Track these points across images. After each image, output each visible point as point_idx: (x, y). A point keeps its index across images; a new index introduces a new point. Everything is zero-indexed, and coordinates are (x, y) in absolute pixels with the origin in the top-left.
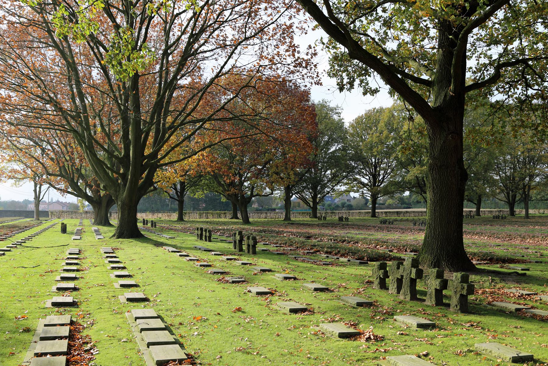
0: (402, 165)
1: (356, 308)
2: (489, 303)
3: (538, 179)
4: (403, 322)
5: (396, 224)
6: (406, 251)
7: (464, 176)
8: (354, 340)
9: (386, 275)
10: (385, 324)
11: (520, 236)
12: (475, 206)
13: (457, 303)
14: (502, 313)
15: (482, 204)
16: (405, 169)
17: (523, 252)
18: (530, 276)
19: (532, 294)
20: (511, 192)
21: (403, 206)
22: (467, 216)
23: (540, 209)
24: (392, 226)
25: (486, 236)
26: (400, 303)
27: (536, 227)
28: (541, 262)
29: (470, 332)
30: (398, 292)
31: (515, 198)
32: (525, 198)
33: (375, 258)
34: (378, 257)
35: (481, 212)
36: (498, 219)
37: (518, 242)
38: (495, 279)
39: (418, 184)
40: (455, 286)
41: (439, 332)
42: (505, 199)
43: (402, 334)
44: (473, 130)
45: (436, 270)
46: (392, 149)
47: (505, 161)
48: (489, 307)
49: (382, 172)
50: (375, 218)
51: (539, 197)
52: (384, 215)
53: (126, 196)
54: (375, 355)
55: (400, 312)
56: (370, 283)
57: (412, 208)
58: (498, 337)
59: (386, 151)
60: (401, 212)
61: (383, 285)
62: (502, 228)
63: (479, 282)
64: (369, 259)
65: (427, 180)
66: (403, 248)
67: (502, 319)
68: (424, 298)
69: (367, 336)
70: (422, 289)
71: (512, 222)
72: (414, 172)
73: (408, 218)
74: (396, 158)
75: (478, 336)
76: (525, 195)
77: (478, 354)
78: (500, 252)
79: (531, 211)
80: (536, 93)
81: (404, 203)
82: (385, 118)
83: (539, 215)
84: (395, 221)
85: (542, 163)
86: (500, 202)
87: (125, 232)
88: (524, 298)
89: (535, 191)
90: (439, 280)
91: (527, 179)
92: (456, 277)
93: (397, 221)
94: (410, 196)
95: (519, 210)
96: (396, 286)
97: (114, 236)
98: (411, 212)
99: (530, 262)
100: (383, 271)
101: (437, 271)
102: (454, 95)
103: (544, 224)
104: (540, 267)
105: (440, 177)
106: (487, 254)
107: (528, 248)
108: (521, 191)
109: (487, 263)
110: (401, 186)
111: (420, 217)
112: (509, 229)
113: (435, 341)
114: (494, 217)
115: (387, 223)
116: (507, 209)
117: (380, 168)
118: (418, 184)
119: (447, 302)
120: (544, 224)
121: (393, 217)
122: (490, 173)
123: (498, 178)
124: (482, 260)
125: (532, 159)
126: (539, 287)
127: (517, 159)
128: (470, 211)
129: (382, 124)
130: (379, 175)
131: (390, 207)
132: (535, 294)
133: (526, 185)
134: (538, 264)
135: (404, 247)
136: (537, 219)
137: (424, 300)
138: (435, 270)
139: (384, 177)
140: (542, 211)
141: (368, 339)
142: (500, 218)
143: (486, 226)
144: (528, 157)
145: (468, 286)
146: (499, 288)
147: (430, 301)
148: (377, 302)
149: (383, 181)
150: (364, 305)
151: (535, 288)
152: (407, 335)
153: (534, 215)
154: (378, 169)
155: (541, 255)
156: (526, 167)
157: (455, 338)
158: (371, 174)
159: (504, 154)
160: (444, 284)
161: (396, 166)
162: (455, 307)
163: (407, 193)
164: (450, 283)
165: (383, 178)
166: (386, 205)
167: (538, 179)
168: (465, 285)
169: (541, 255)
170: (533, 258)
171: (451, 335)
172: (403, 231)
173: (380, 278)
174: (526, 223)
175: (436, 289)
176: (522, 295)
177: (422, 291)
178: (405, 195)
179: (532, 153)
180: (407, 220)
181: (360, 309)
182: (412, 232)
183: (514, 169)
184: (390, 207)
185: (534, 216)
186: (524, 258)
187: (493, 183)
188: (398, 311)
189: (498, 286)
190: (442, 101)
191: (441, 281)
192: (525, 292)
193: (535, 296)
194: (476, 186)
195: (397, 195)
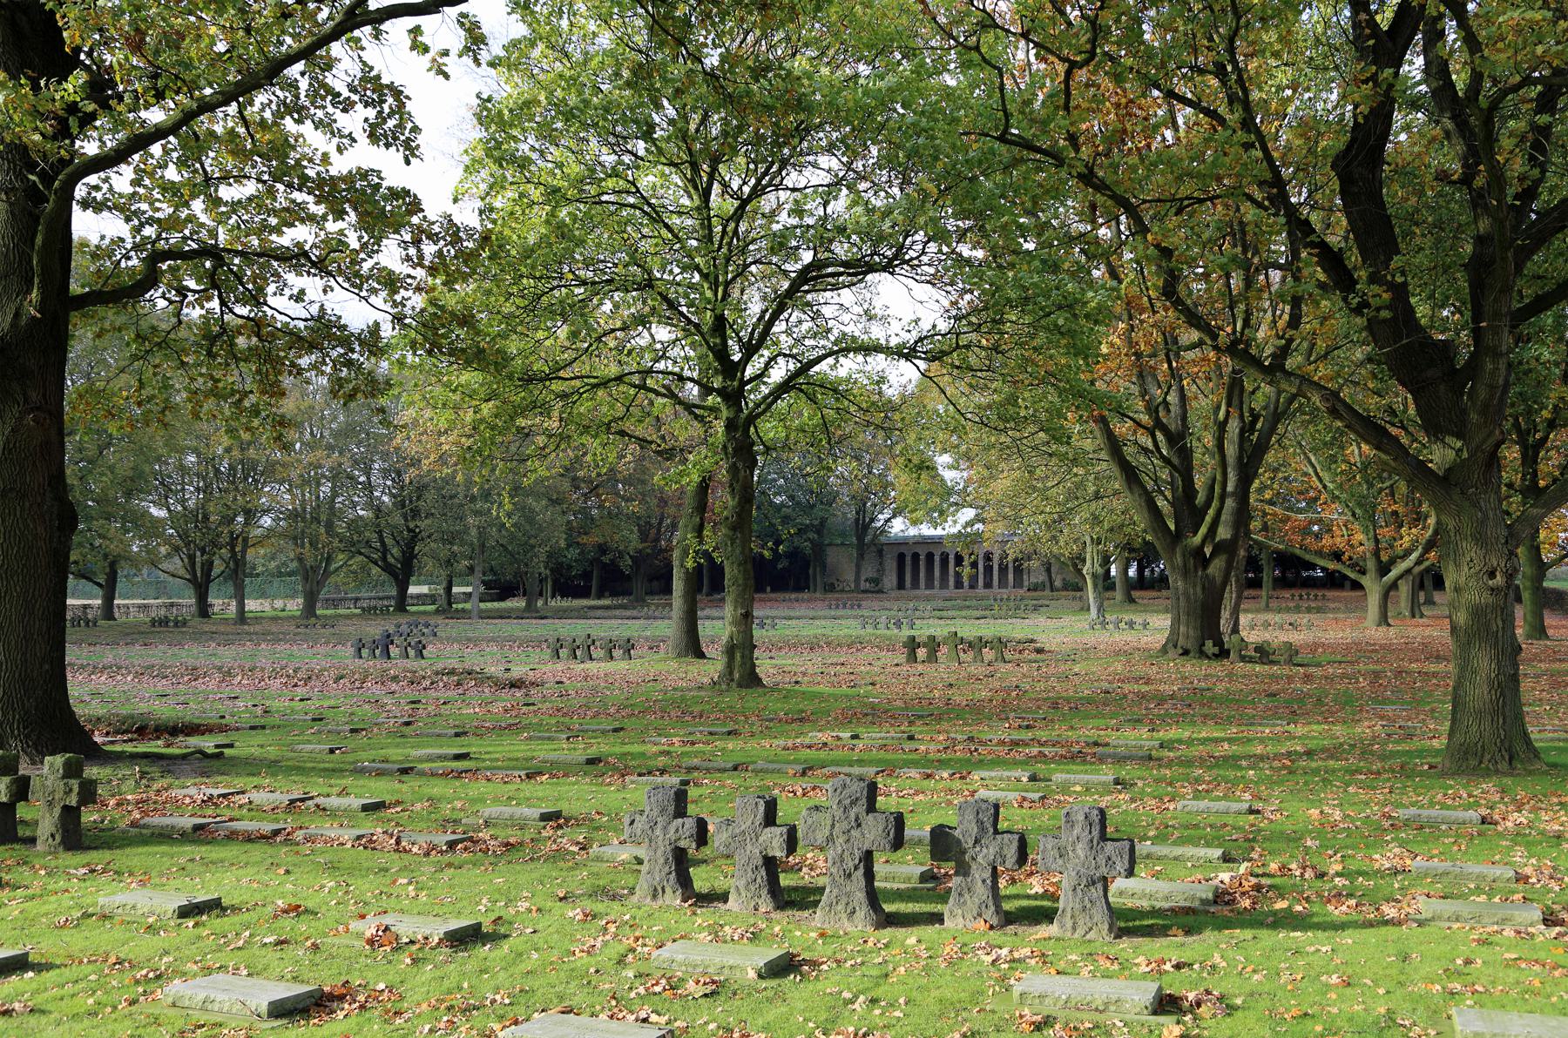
2: (134, 824)
3: (267, 521)
7: (67, 518)
11: (220, 669)
13: (53, 829)
14: (164, 836)
15: (121, 585)
18: (232, 758)
19: (232, 794)
20: (198, 553)
22: (76, 622)
23: (274, 597)
25: (130, 672)
27: (263, 646)
28: (263, 727)
29: (88, 883)
31: (210, 570)
32: (235, 571)
35: (116, 610)
37: (213, 685)
40: (51, 789)
42: (182, 572)
44: (91, 393)
47: (183, 469)
51: (273, 564)
58: (152, 881)
62: (176, 649)
71: (202, 633)
75: (107, 887)
76: (237, 562)
77: (104, 917)
78: (165, 711)
79: (251, 605)
80: (246, 324)
86: (171, 579)
91: (240, 519)
92: (52, 765)
95: (221, 602)
99: (238, 729)
102: (39, 315)
103: (281, 636)
104: (259, 738)
106: (131, 716)
107: (236, 698)
112: (192, 653)
116: (189, 600)
119: (28, 833)
120: (281, 636)
122: (141, 500)
123: (163, 513)
124: (117, 732)
127: (214, 466)
128: (85, 607)
132: (238, 793)
133: (238, 536)
134: (254, 732)
136: (266, 626)
140: (279, 604)
142: (172, 624)
143: (130, 648)
144: (242, 462)
145: (81, 785)
146: (158, 791)
155: (266, 712)
157: (53, 898)
162: (50, 840)
167: (267, 521)
168: (75, 784)
169: (266, 712)
171: (41, 895)
174: (238, 637)
176: (211, 797)
183: (204, 492)
185: (262, 618)
186: (223, 721)
187: (152, 529)
191: (12, 782)
192: (216, 792)
193: (237, 797)
194: (100, 536)
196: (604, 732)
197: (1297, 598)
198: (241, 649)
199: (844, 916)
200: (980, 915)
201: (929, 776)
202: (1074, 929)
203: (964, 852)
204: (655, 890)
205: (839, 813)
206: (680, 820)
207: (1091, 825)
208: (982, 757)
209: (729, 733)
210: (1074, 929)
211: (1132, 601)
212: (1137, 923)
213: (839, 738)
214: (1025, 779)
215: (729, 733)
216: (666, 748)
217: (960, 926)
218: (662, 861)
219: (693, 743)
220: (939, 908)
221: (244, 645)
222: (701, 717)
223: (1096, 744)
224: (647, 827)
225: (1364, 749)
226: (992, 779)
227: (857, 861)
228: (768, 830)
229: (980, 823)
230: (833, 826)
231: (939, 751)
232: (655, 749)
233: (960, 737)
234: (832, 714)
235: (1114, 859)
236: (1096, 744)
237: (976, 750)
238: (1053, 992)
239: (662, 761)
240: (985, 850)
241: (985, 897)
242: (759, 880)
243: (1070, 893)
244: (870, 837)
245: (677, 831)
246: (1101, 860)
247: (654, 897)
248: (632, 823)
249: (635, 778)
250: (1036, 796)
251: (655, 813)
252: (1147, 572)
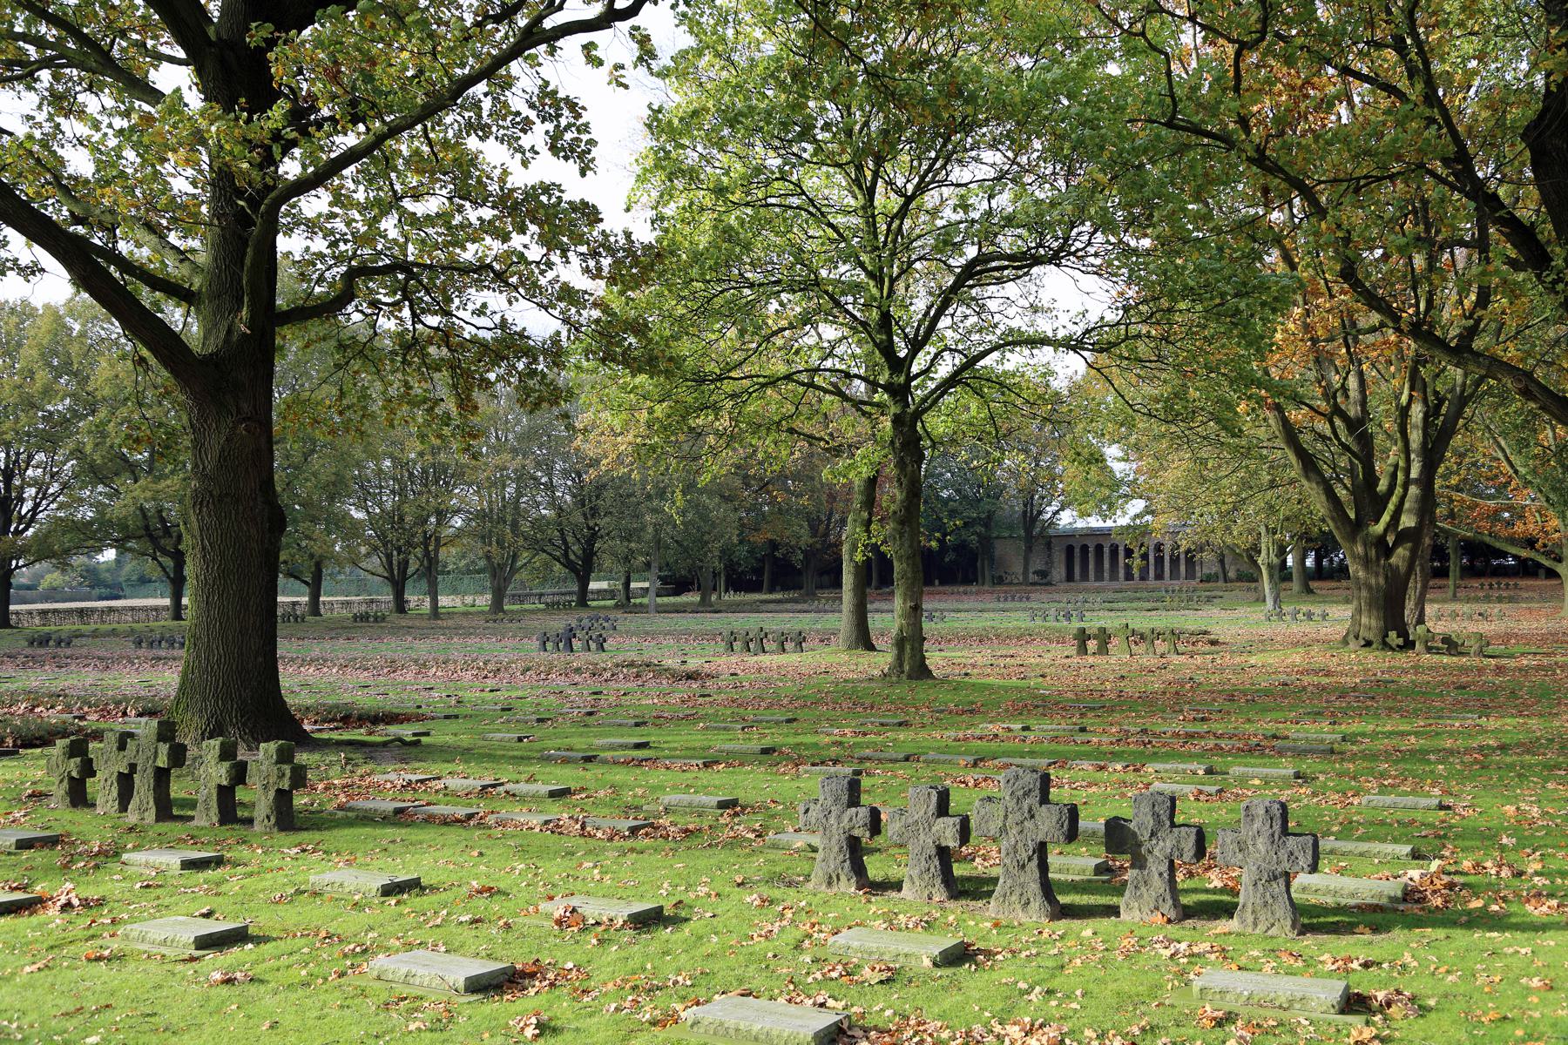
0: (94, 473)
1: (15, 854)
2: (341, 808)
3: (458, 522)
4: (147, 865)
5: (81, 647)
6: (125, 714)
7: (277, 520)
8: (31, 915)
9: (88, 770)
10: (100, 875)
11: (416, 661)
12: (306, 589)
13: (269, 811)
14: (366, 819)
16: (106, 485)
17: (419, 698)
18: (429, 746)
19: (429, 779)
21: (97, 591)
23: (465, 593)
24: (69, 652)
26: (131, 829)
28: (457, 717)
30: (123, 807)
32: (429, 569)
33: (37, 739)
34: (47, 736)
36: (365, 620)
37: (410, 676)
38: (353, 756)
39: (147, 528)
40: (265, 774)
41: (233, 871)
42: (381, 570)
43: (148, 886)
45: (218, 743)
46: (65, 423)
48: (340, 814)
49: (30, 492)
50: (8, 631)
52: (37, 620)
54: (91, 932)
55: (134, 847)
56: (37, 796)
57: (125, 597)
59: (44, 430)
60: (93, 610)
61: (78, 796)
62: (376, 643)
63: (318, 767)
64: (19, 742)
65: (186, 528)
66: (119, 705)
67: (368, 830)
68: (190, 813)
69: (63, 900)
70: (183, 795)
72: (133, 495)
73: (115, 626)
74: (78, 453)
76: (430, 560)
77: (315, 894)
78: (366, 701)
81: (98, 583)
82: (38, 332)
83: (463, 609)
84: (77, 637)
85: (466, 483)
88: (414, 789)
89: (453, 551)
90: (227, 764)
91: (433, 519)
92: (266, 751)
93: (82, 636)
94: (117, 561)
96: (115, 793)
98: (124, 608)
99: (433, 718)
100: (79, 759)
101: (222, 744)
104: (453, 726)
105: (220, 524)
106: (337, 706)
108: (419, 551)
109: (337, 728)
110: (90, 536)
111: (151, 624)
112: (390, 647)
113: (223, 888)
114: (355, 617)
116: (387, 597)
117: (23, 480)
118: (147, 528)
119: (246, 814)
121: (69, 626)
124: (324, 721)
125: (440, 470)
126: (446, 765)
128: (294, 604)
129: (29, 353)
130: (21, 500)
131: (52, 594)
132: (434, 779)
134: (448, 721)
135: (118, 703)
137: (192, 818)
138: (216, 743)
139: (37, 505)
140: (469, 599)
141: (68, 906)
144: (433, 465)
146: (362, 776)
147: (205, 817)
148: (69, 835)
149: (33, 519)
150: (37, 844)
151: (436, 768)
152: (160, 886)
154: (17, 482)
156: (429, 492)
157: (269, 876)
159: (377, 458)
160: (239, 774)
161: (76, 476)
163: (110, 555)
164: (251, 768)
165: (35, 510)
166: (40, 589)
167: (458, 522)
168: (287, 769)
170: (441, 709)
172: (106, 664)
173: (71, 779)
175: (220, 787)
177: (184, 799)
178: (100, 558)
179: (442, 457)
180: (114, 633)
181: (26, 854)
182: (133, 664)
184: (52, 594)
186: (420, 711)
187: (352, 530)
188: (130, 846)
189: (360, 771)
190: (220, 342)
191: (232, 767)
192: (414, 778)
193: (434, 783)
195: (78, 560)
196: (777, 723)
197: (1487, 587)
199: (1018, 906)
200: (1157, 908)
201: (1102, 768)
202: (1255, 924)
203: (1140, 845)
204: (830, 877)
205: (1012, 804)
206: (854, 810)
207: (1271, 819)
208: (1156, 750)
209: (900, 724)
210: (1255, 924)
211: (1310, 591)
212: (1322, 920)
213: (1010, 730)
214: (1201, 772)
215: (900, 724)
216: (838, 738)
217: (1137, 919)
218: (836, 849)
219: (865, 734)
220: (1114, 900)
222: (872, 708)
223: (1275, 737)
224: (821, 816)
226: (1166, 771)
227: (1030, 853)
228: (941, 819)
229: (1156, 816)
230: (1006, 817)
231: (1112, 743)
232: (827, 739)
233: (1133, 729)
234: (1003, 706)
235: (1296, 854)
236: (1275, 737)
237: (1150, 742)
238: (1235, 988)
239: (834, 751)
240: (1161, 843)
241: (1162, 890)
242: (932, 870)
243: (1251, 888)
244: (1044, 828)
245: (851, 819)
246: (1283, 855)
247: (830, 884)
248: (807, 811)
249: (808, 767)
250: (1213, 789)
251: (829, 802)
252: (1325, 562)
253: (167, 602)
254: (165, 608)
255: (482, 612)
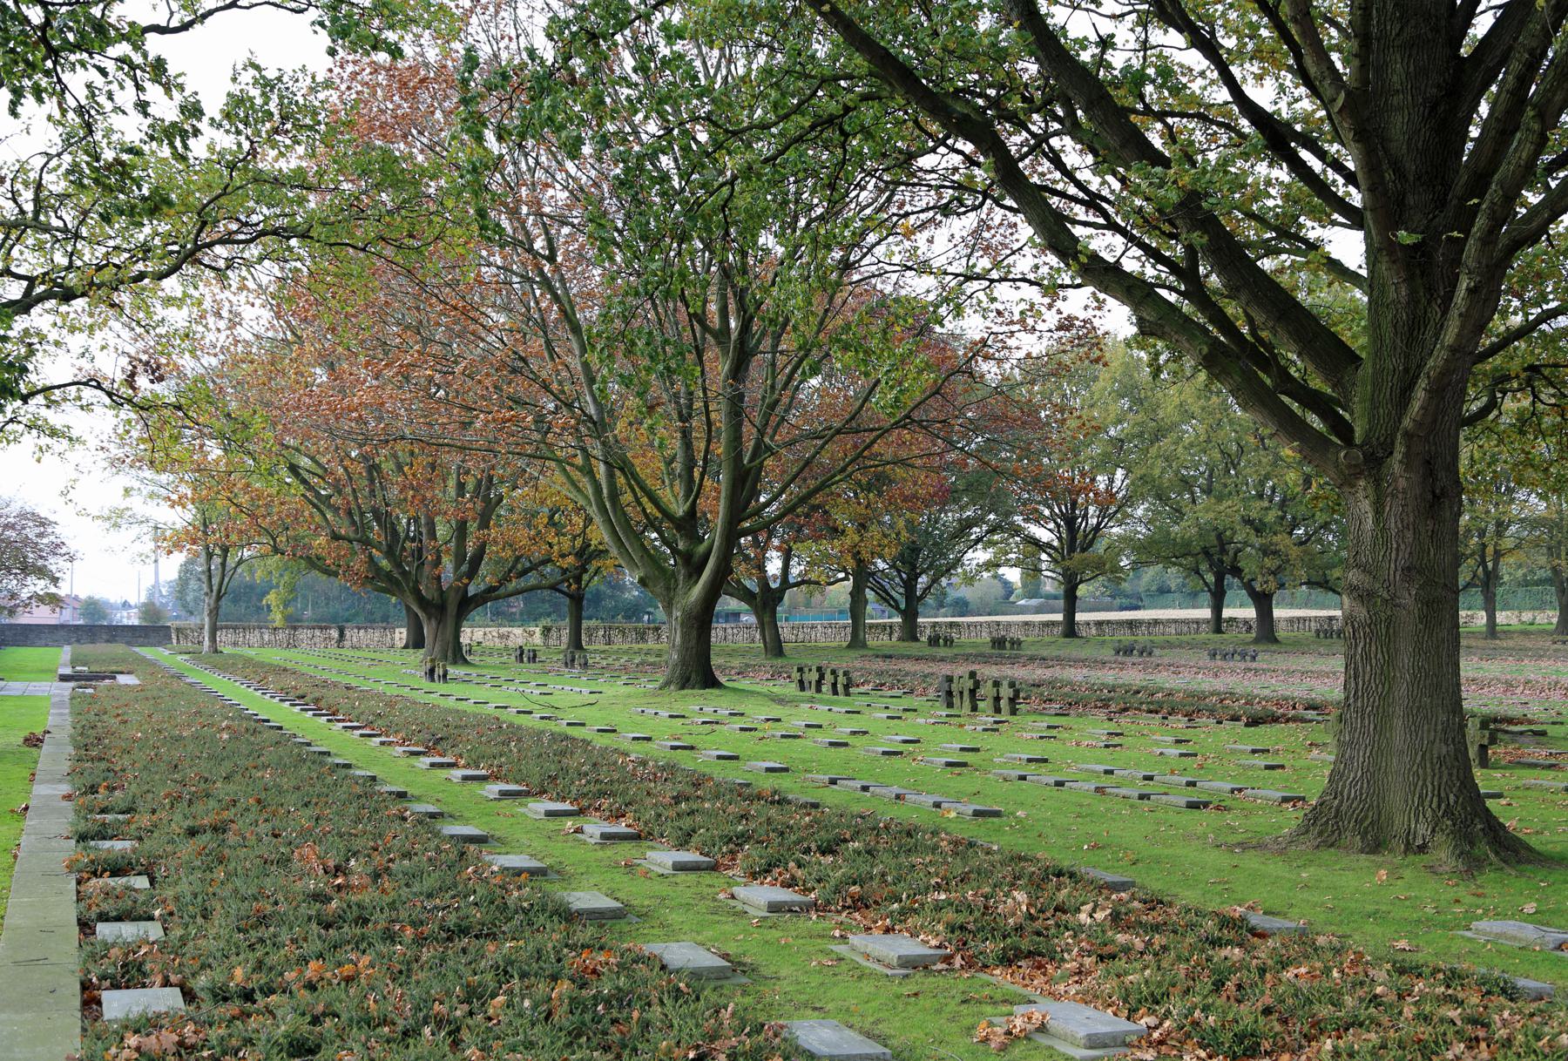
21: (1118, 601)
53: (696, 601)
57: (1144, 608)
79: (1501, 617)
87: (693, 676)
97: (667, 684)
115: (1135, 652)
128: (1331, 618)
140: (1527, 616)
153: (1506, 628)
158: (1063, 516)
198: (1505, 664)
221: (1506, 660)
225: (1372, 239)
253: (1206, 613)
254: (1207, 621)
255: (1550, 633)
